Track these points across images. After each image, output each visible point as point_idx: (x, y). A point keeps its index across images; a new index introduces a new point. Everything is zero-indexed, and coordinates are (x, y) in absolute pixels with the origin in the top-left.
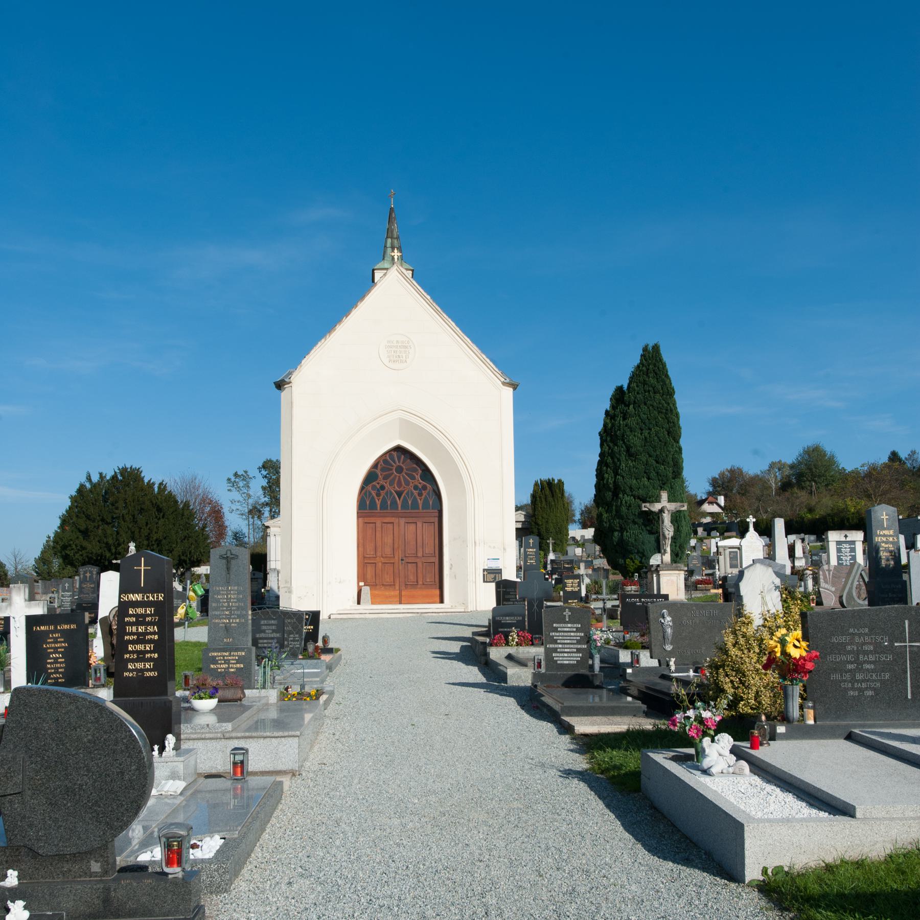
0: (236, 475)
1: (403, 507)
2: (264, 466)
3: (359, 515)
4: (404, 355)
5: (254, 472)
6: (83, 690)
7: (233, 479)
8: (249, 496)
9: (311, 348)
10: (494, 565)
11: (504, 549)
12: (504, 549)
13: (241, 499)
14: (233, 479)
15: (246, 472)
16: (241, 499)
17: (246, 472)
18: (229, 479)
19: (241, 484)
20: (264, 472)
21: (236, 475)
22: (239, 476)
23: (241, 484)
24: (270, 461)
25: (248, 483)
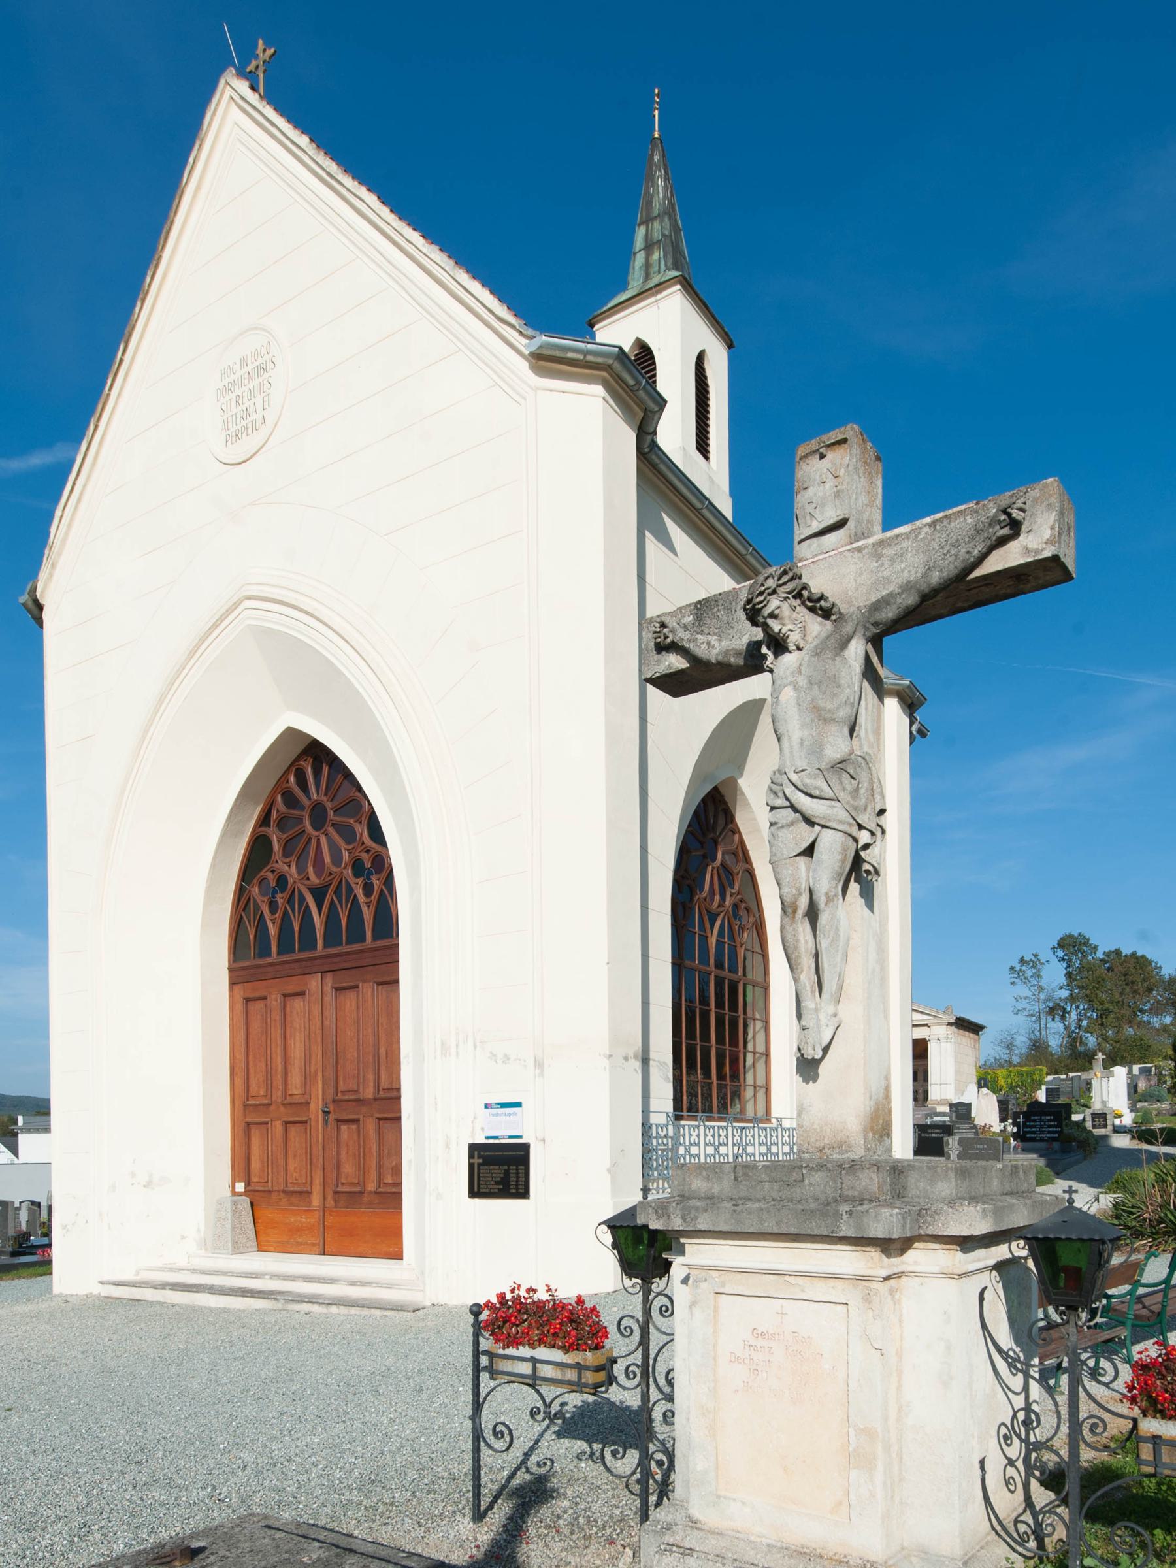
0: (1022, 961)
1: (332, 937)
2: (1061, 944)
3: (239, 975)
4: (258, 400)
5: (1046, 954)
6: (45, 1305)
7: (1018, 967)
8: (1041, 989)
9: (47, 518)
10: (502, 1129)
11: (539, 1064)
12: (539, 1064)
13: (1029, 994)
14: (1018, 967)
15: (1036, 956)
16: (1029, 994)
17: (1036, 956)
18: (1012, 968)
19: (1029, 973)
20: (1060, 953)
21: (1022, 961)
22: (1028, 963)
23: (1029, 973)
24: (1070, 936)
25: (1039, 970)
